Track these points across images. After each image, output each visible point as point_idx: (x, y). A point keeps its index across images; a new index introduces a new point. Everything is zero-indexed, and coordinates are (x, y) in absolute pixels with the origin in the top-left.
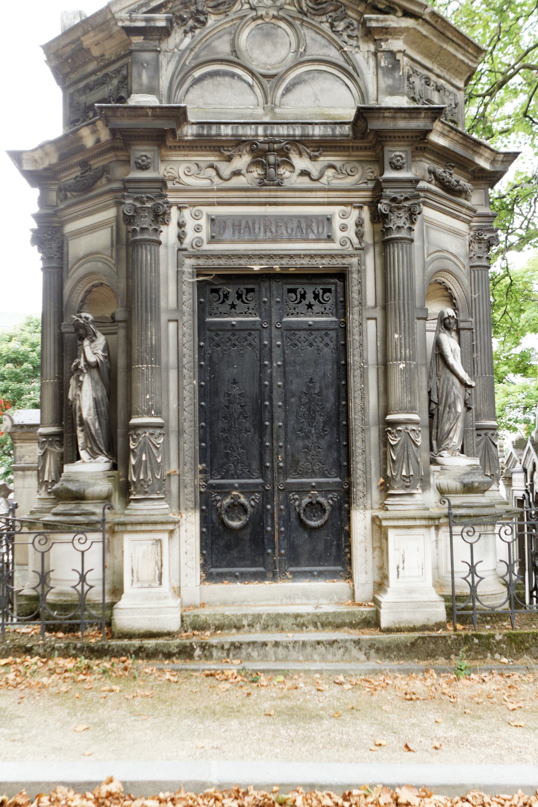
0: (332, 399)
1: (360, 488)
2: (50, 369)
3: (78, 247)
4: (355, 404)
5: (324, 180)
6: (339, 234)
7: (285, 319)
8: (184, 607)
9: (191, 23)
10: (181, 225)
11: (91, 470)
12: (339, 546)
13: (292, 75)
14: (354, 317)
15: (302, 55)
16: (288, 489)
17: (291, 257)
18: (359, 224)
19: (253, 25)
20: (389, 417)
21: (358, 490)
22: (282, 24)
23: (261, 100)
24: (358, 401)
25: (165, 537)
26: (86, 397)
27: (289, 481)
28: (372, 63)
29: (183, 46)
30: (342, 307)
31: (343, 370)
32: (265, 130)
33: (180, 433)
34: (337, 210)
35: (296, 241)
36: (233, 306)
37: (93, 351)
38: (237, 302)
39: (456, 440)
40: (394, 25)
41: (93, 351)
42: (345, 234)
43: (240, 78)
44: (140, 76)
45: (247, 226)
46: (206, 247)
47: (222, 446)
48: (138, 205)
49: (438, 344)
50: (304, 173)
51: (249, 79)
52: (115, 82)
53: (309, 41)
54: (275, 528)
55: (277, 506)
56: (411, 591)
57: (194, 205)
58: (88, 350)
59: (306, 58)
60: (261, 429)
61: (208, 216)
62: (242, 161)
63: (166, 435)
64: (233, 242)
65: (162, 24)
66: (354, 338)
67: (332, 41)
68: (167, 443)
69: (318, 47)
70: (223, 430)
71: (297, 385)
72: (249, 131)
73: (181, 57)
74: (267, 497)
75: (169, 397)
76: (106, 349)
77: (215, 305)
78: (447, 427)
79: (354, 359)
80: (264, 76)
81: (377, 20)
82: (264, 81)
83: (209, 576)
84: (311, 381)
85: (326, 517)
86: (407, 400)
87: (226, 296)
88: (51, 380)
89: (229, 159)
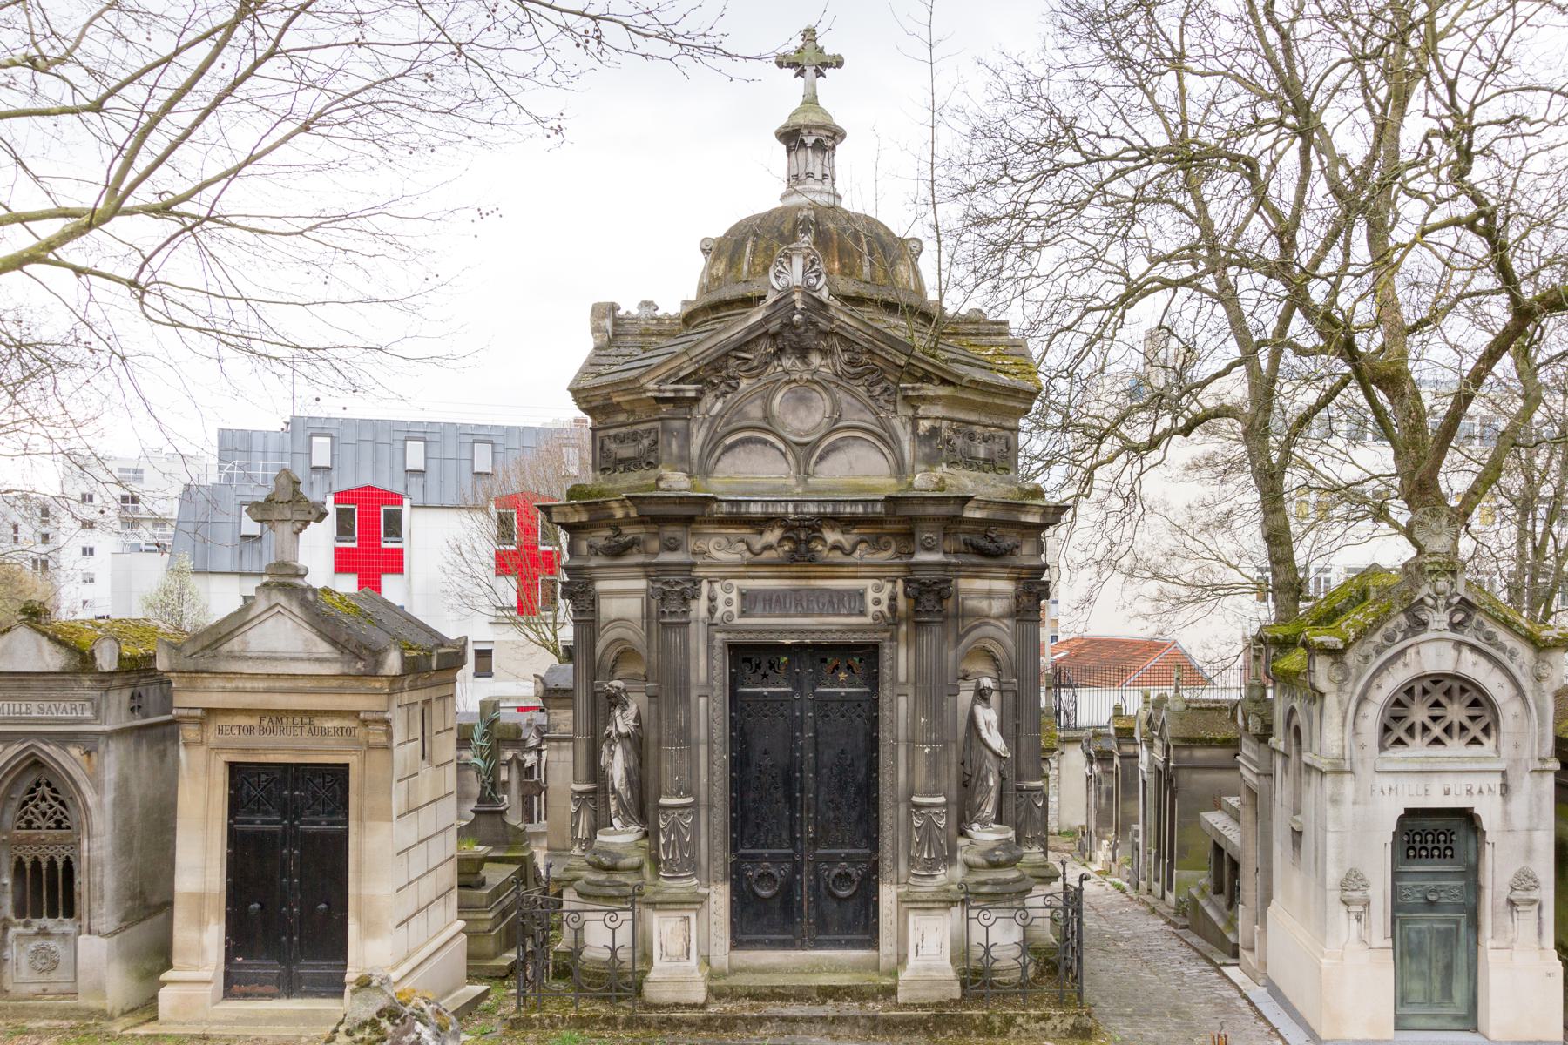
0: (863, 770)
1: (888, 862)
2: (582, 738)
3: (610, 608)
4: (885, 779)
5: (857, 554)
6: (872, 608)
7: (819, 690)
8: (712, 976)
9: (723, 387)
10: (712, 599)
11: (621, 837)
12: (867, 916)
13: (827, 442)
14: (885, 692)
15: (837, 421)
16: (818, 860)
17: (823, 632)
18: (893, 598)
19: (787, 388)
20: (915, 799)
21: (886, 865)
22: (816, 387)
23: (794, 469)
24: (887, 777)
25: (693, 916)
26: (617, 766)
27: (819, 851)
28: (909, 428)
29: (714, 412)
30: (873, 680)
31: (873, 744)
32: (795, 507)
33: (710, 807)
34: (870, 582)
35: (828, 615)
36: (765, 676)
37: (623, 722)
38: (770, 672)
39: (989, 810)
40: (930, 393)
41: (623, 722)
42: (878, 608)
43: (773, 445)
44: (670, 445)
45: (778, 601)
46: (737, 621)
47: (752, 816)
48: (667, 589)
49: (972, 719)
50: (836, 547)
51: (781, 446)
52: (646, 442)
53: (844, 405)
54: (805, 897)
55: (806, 877)
56: (929, 969)
57: (725, 578)
58: (619, 720)
59: (841, 424)
60: (790, 799)
61: (739, 590)
62: (772, 536)
63: (696, 815)
64: (763, 616)
65: (692, 394)
66: (885, 714)
67: (867, 407)
68: (696, 823)
69: (856, 414)
70: (754, 801)
71: (828, 756)
72: (780, 509)
73: (712, 423)
74: (797, 868)
75: (700, 775)
76: (638, 718)
77: (748, 673)
78: (978, 800)
79: (884, 735)
80: (797, 444)
81: (913, 389)
82: (797, 449)
83: (737, 943)
84: (843, 752)
85: (854, 888)
86: (931, 783)
87: (758, 666)
88: (582, 748)
89: (761, 533)
